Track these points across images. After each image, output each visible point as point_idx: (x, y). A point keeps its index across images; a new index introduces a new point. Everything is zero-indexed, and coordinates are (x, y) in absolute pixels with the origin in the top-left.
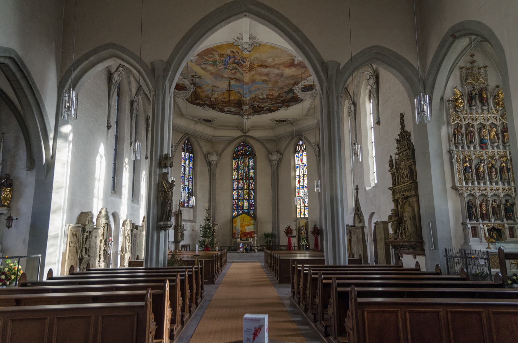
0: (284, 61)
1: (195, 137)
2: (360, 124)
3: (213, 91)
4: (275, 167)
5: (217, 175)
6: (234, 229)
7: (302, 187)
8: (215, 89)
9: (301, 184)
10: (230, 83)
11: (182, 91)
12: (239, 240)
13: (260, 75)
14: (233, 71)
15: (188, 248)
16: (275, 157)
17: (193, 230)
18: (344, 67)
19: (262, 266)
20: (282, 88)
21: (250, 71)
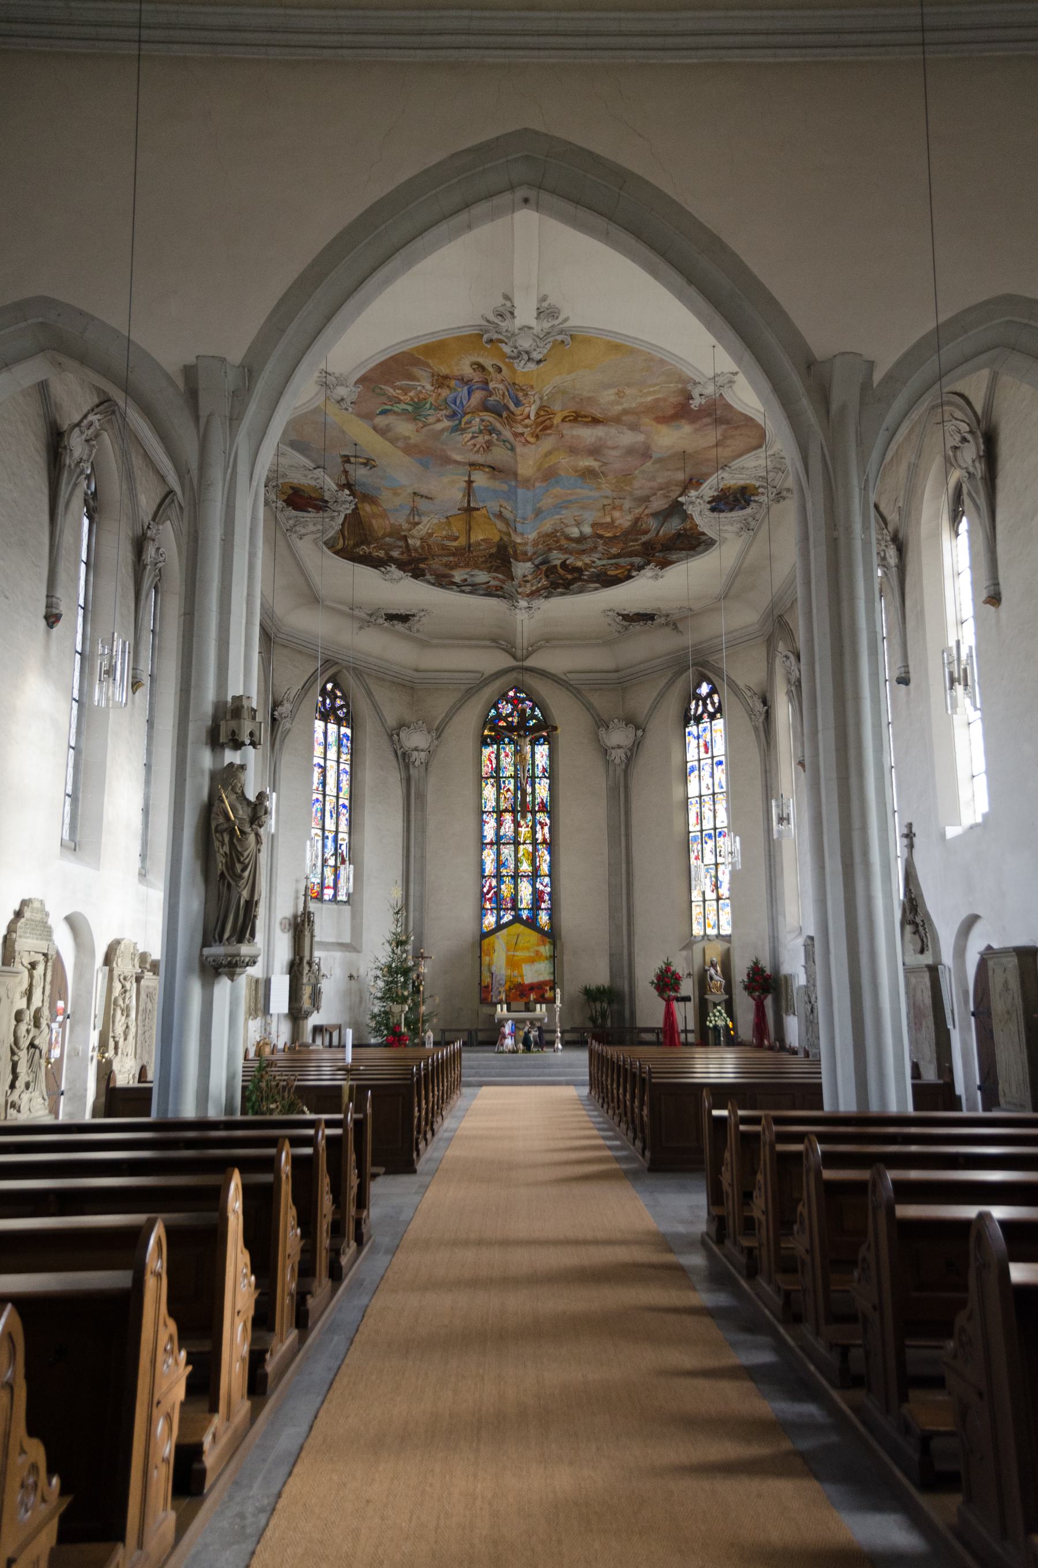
0: (657, 400)
1: (358, 673)
2: (922, 612)
3: (414, 511)
4: (620, 771)
5: (430, 798)
6: (486, 974)
7: (710, 836)
8: (423, 505)
9: (708, 825)
10: (470, 482)
11: (311, 515)
12: (501, 1011)
13: (573, 450)
14: (481, 439)
15: (335, 1035)
16: (619, 737)
17: (351, 977)
18: (889, 378)
19: (580, 1099)
20: (646, 499)
21: (537, 437)
